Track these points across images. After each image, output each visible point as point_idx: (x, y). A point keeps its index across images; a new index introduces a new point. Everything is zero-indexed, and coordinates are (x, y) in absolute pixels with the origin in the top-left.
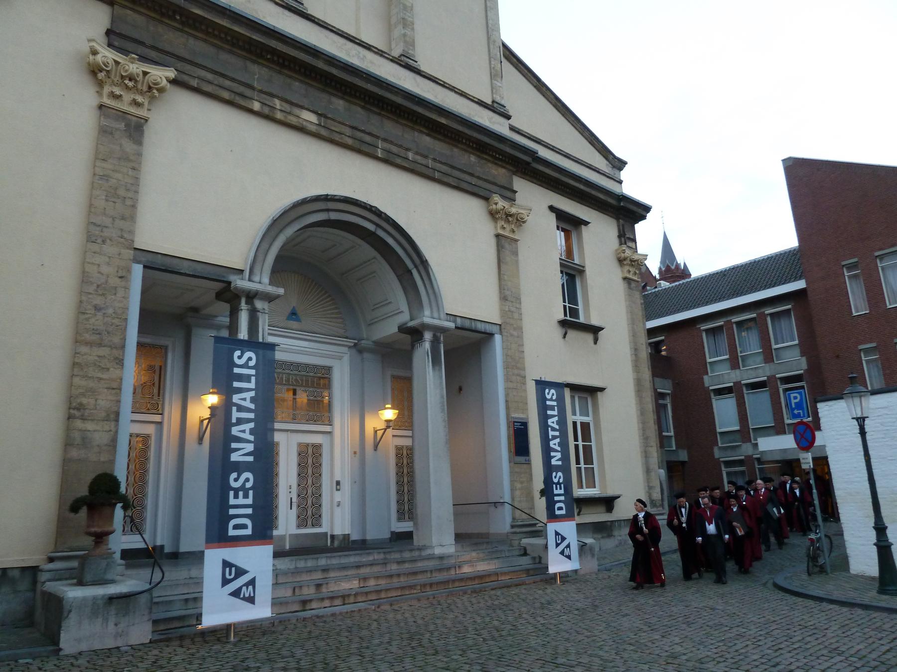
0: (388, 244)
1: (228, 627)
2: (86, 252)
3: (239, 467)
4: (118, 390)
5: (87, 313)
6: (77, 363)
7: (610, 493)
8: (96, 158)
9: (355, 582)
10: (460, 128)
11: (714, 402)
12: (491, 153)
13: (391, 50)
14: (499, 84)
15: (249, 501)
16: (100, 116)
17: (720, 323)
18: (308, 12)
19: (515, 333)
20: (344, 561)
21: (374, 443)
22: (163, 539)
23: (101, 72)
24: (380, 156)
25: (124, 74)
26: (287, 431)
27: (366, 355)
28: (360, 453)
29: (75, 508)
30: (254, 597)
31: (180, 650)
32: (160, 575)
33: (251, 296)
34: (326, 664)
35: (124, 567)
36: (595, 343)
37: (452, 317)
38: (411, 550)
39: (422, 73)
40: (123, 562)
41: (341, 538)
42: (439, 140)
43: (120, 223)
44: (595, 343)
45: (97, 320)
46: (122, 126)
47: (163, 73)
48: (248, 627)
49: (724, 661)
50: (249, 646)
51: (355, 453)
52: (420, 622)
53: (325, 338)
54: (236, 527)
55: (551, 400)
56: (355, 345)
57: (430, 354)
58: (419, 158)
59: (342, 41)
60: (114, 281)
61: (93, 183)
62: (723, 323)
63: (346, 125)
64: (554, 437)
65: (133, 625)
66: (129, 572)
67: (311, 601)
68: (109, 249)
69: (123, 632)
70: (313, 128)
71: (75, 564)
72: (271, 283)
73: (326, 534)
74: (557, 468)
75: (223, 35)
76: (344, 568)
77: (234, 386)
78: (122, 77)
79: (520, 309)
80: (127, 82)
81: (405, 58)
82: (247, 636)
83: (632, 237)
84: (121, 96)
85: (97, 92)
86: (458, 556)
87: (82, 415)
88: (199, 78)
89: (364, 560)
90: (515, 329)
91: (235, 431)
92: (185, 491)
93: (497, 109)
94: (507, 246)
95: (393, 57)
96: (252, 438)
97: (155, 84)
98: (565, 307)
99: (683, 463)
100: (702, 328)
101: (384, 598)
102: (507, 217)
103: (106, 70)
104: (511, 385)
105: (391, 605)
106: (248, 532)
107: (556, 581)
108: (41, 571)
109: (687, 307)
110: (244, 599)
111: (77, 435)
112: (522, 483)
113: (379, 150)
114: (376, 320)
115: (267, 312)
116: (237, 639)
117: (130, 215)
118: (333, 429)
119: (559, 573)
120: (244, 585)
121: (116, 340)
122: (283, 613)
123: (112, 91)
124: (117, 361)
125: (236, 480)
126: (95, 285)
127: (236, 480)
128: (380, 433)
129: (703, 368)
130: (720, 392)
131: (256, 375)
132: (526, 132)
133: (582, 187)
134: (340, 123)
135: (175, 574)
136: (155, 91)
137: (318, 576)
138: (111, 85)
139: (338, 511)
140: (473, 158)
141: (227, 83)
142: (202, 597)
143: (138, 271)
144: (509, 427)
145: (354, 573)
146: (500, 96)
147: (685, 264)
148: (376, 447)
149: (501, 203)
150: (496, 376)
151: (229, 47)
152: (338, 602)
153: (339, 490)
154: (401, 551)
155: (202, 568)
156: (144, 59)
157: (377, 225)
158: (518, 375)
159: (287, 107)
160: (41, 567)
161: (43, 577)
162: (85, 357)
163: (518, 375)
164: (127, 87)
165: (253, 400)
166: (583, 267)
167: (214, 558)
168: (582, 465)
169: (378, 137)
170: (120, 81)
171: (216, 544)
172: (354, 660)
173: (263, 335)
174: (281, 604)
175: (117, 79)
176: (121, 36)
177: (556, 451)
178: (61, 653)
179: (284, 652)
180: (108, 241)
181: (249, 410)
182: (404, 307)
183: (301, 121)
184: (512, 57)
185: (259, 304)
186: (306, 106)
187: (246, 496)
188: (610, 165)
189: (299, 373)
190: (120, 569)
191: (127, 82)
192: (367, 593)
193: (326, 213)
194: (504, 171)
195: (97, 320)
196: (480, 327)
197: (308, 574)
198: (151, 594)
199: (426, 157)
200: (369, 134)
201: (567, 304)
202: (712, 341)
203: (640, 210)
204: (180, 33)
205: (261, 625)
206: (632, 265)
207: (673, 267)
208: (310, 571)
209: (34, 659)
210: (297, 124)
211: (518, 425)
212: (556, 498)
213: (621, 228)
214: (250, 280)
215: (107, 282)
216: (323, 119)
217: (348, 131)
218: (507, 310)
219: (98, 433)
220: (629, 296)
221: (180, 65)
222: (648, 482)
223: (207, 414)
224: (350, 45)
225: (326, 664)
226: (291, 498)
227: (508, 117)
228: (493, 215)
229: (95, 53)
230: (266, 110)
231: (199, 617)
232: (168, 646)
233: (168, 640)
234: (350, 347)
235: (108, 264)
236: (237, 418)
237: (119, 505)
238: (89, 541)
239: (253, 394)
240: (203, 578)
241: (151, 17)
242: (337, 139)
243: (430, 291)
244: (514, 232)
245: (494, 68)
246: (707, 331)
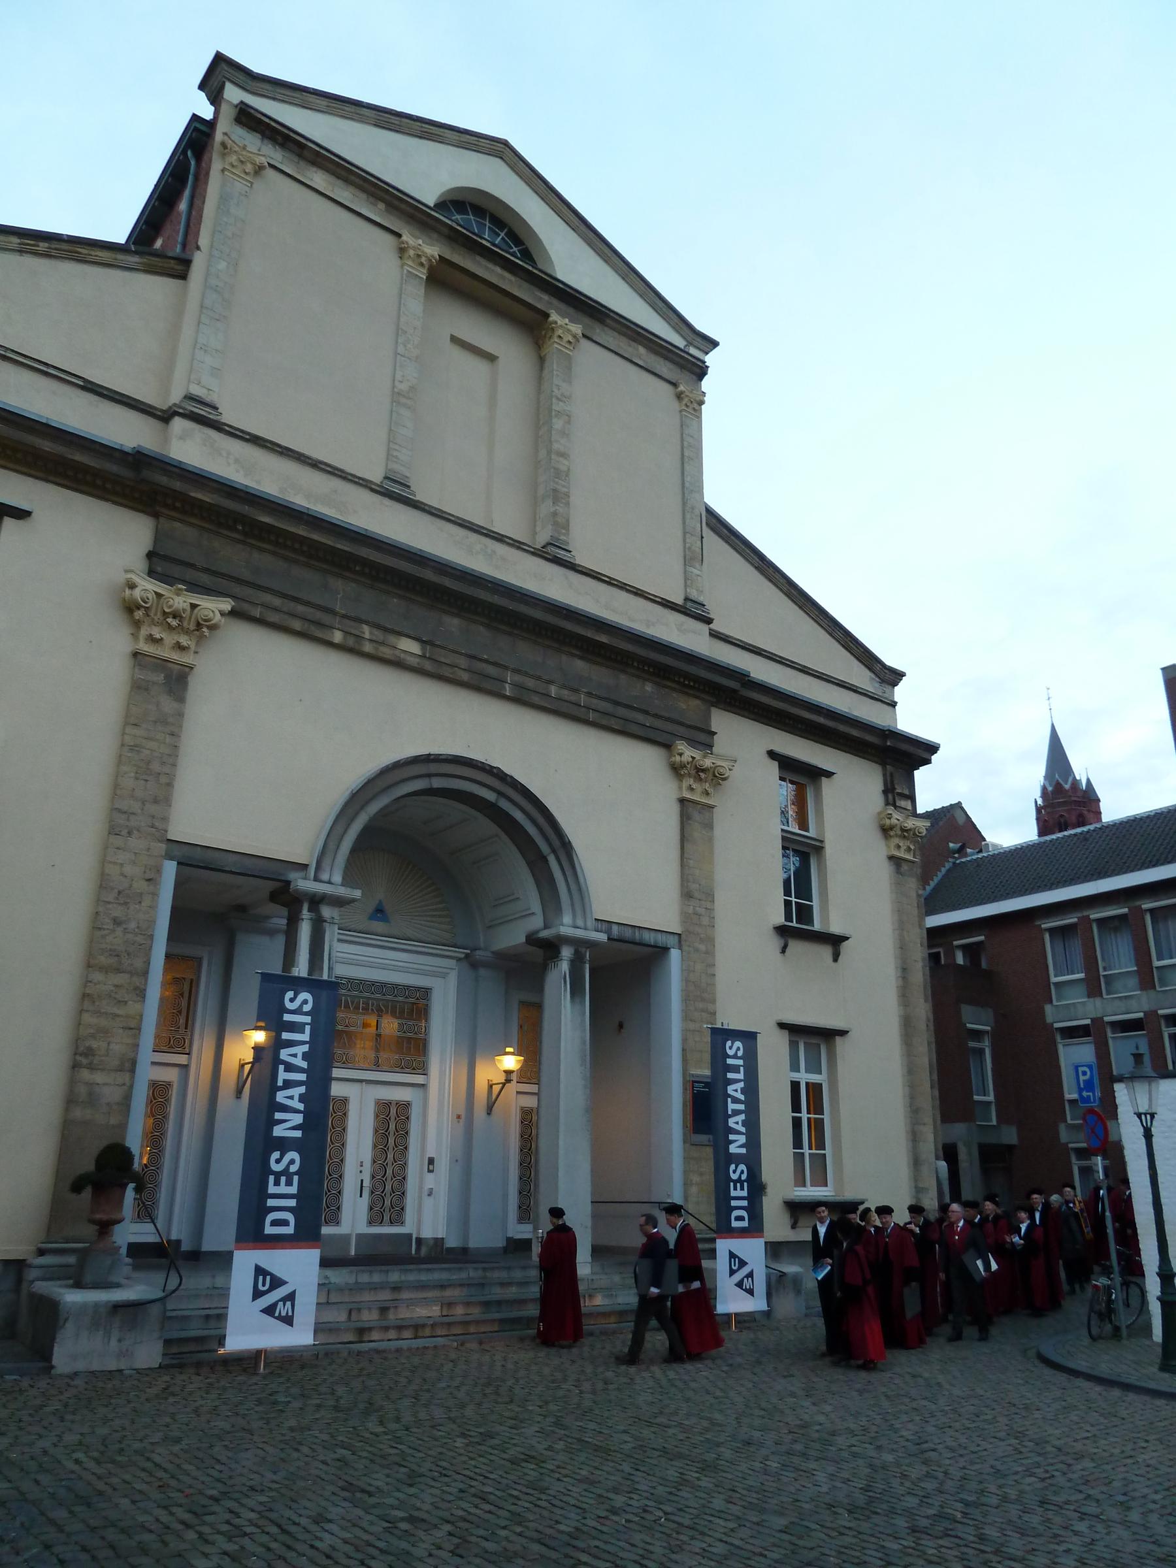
1: (259, 1353)
3: (283, 1145)
5: (104, 929)
6: (88, 995)
8: (126, 724)
9: (434, 1308)
11: (1061, 1048)
14: (696, 571)
15: (293, 1190)
16: (134, 666)
17: (1071, 920)
18: (417, 498)
19: (702, 947)
20: (424, 1277)
22: (179, 1231)
23: (139, 609)
25: (167, 610)
26: (361, 1081)
27: (482, 972)
28: (466, 1118)
29: (77, 1187)
33: (316, 901)
34: (370, 1404)
35: (131, 1267)
36: (835, 959)
37: (605, 925)
38: (524, 1268)
39: (577, 568)
41: (432, 1242)
43: (153, 809)
44: (835, 959)
46: (160, 678)
48: (283, 1357)
50: (281, 1380)
51: (459, 1117)
52: (510, 1366)
53: (424, 947)
54: (275, 1223)
55: (735, 1057)
56: (467, 956)
58: (565, 693)
59: (462, 532)
60: (140, 886)
61: (120, 756)
62: (1076, 920)
63: (461, 654)
64: (736, 1113)
66: (136, 1275)
67: (370, 1329)
68: (135, 843)
70: (413, 661)
71: (72, 1260)
72: (344, 884)
74: (738, 1159)
75: (297, 546)
76: (423, 1287)
77: (284, 1019)
78: (164, 613)
79: (710, 910)
80: (169, 620)
82: (281, 1368)
83: (906, 792)
85: (132, 634)
86: (593, 1280)
87: (91, 1063)
89: (454, 1277)
90: (702, 941)
91: (280, 1097)
94: (696, 816)
96: (301, 1107)
97: (206, 621)
98: (788, 904)
99: (1010, 1148)
100: (1043, 926)
101: (473, 1334)
102: (697, 772)
104: (692, 1026)
105: (481, 1343)
106: (289, 1230)
107: (730, 1327)
108: (30, 1266)
109: (1020, 891)
110: (280, 1318)
111: (82, 1090)
112: (701, 1174)
113: (507, 686)
116: (267, 1371)
117: (163, 798)
119: (735, 1314)
121: (138, 964)
123: (151, 635)
124: (138, 992)
125: (278, 1161)
126: (116, 891)
127: (278, 1161)
128: (496, 1089)
129: (1044, 991)
130: (1072, 1033)
131: (312, 1024)
132: (738, 640)
135: (197, 1281)
136: (205, 630)
137: (385, 1295)
138: (149, 626)
139: (428, 1202)
140: (649, 687)
141: (301, 609)
142: (227, 1314)
143: (170, 869)
144: (685, 1089)
147: (1088, 781)
149: (687, 752)
152: (407, 1334)
154: (509, 1268)
155: (229, 1276)
156: (195, 587)
159: (379, 635)
161: (32, 1274)
162: (97, 986)
166: (822, 842)
167: (245, 1261)
169: (506, 668)
170: (162, 618)
171: (251, 1244)
173: (330, 955)
174: (330, 1330)
175: (158, 617)
177: (738, 1133)
178: (53, 1372)
179: (323, 1389)
181: (299, 1070)
182: (536, 906)
183: (397, 652)
184: (722, 528)
185: (326, 912)
190: (126, 1270)
192: (449, 1324)
194: (697, 702)
196: (649, 938)
197: (372, 1292)
198: (165, 1305)
201: (793, 899)
203: (919, 751)
206: (905, 837)
207: (1067, 787)
210: (392, 658)
211: (699, 1087)
213: (889, 779)
214: (316, 879)
216: (428, 647)
217: (463, 662)
219: (107, 1085)
220: (898, 885)
221: (238, 590)
222: (916, 1180)
223: (249, 1056)
225: (370, 1404)
226: (362, 1181)
227: (709, 621)
228: (677, 770)
229: (132, 586)
230: (351, 642)
231: (221, 1340)
232: (181, 1373)
233: (181, 1366)
234: (459, 960)
236: (284, 1080)
237: (131, 1186)
238: (90, 1231)
239: (306, 1048)
240: (230, 1288)
241: (204, 528)
243: (573, 887)
244: (707, 794)
245: (689, 548)
246: (1052, 931)
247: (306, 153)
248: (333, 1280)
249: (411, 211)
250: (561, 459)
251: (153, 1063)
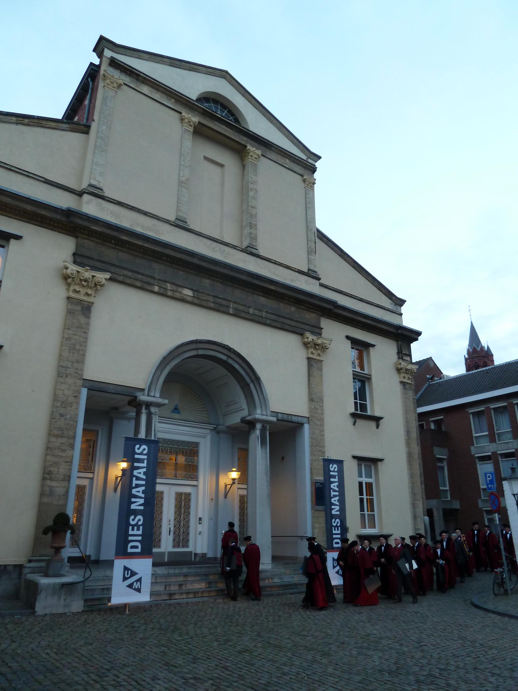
0: (235, 367)
1: (125, 605)
2: (57, 383)
3: (135, 513)
4: (70, 463)
6: (49, 447)
7: (385, 532)
8: (64, 328)
10: (284, 291)
11: (478, 465)
12: (305, 305)
13: (242, 247)
15: (140, 532)
16: (68, 303)
17: (482, 408)
19: (318, 423)
21: (225, 493)
22: (90, 551)
24: (231, 313)
25: (82, 278)
27: (221, 435)
28: (215, 500)
29: (45, 532)
30: (140, 588)
31: (98, 616)
32: (90, 573)
33: (148, 405)
34: (175, 627)
35: (69, 567)
36: (377, 427)
40: (68, 564)
42: (271, 299)
44: (377, 427)
45: (61, 422)
46: (79, 308)
47: (103, 276)
48: (137, 607)
49: (447, 651)
51: (212, 499)
54: (132, 547)
55: (334, 471)
56: (215, 428)
60: (71, 399)
62: (484, 408)
64: (335, 496)
65: (74, 601)
66: (71, 571)
67: (174, 594)
68: (70, 380)
69: (68, 604)
70: (189, 299)
71: (43, 564)
72: (161, 397)
73: (192, 552)
78: (81, 280)
79: (322, 406)
80: (83, 283)
81: (250, 249)
83: (407, 353)
84: (80, 291)
88: (123, 275)
91: (134, 491)
92: (105, 522)
93: (312, 274)
94: (315, 365)
95: (242, 249)
96: (143, 496)
98: (356, 403)
99: (457, 510)
100: (469, 411)
102: (315, 346)
103: (72, 277)
106: (139, 550)
108: (25, 567)
110: (135, 589)
111: (47, 489)
112: (320, 523)
114: (229, 413)
115: (157, 414)
117: (81, 360)
118: (198, 483)
120: (135, 581)
121: (71, 433)
122: (158, 600)
125: (133, 520)
127: (133, 520)
128: (229, 487)
130: (483, 459)
133: (369, 322)
134: (206, 294)
135: (98, 573)
136: (98, 286)
137: (181, 579)
139: (199, 537)
140: (293, 309)
141: (140, 277)
142: (112, 588)
143: (84, 392)
145: (194, 579)
146: (313, 266)
147: (488, 347)
148: (226, 496)
149: (310, 337)
150: (304, 452)
151: (142, 255)
152: (191, 596)
155: (112, 571)
158: (320, 451)
159: (174, 288)
160: (25, 565)
161: (26, 571)
163: (320, 451)
164: (83, 286)
165: (145, 473)
166: (370, 376)
167: (119, 564)
168: (366, 512)
169: (230, 301)
172: (191, 626)
173: (155, 427)
175: (78, 281)
176: (81, 256)
177: (336, 505)
178: (36, 614)
180: (69, 376)
181: (142, 479)
182: (245, 406)
183: (182, 295)
186: (186, 286)
187: (138, 529)
188: (393, 303)
189: (178, 447)
190: (67, 568)
191: (83, 283)
193: (196, 350)
194: (314, 315)
195: (61, 422)
196: (295, 419)
198: (84, 584)
199: (261, 311)
200: (224, 299)
201: (358, 401)
202: (477, 420)
203: (413, 334)
204: (114, 250)
205: (144, 606)
207: (479, 349)
208: (176, 576)
209: (22, 616)
210: (180, 298)
211: (318, 485)
212: (334, 536)
213: (399, 348)
214: (148, 395)
215: (67, 399)
217: (211, 299)
218: (313, 407)
219: (58, 488)
221: (112, 269)
223: (120, 474)
224: (215, 244)
225: (175, 627)
226: (170, 528)
227: (319, 279)
228: (306, 345)
229: (66, 268)
230: (162, 291)
231: (109, 600)
232: (92, 614)
234: (211, 430)
235: (69, 389)
237: (69, 531)
238: (52, 551)
239: (145, 470)
242: (205, 305)
243: (261, 397)
244: (319, 355)
246: (473, 414)
247: (140, 78)
248: (158, 572)
249: (186, 102)
251: (78, 477)
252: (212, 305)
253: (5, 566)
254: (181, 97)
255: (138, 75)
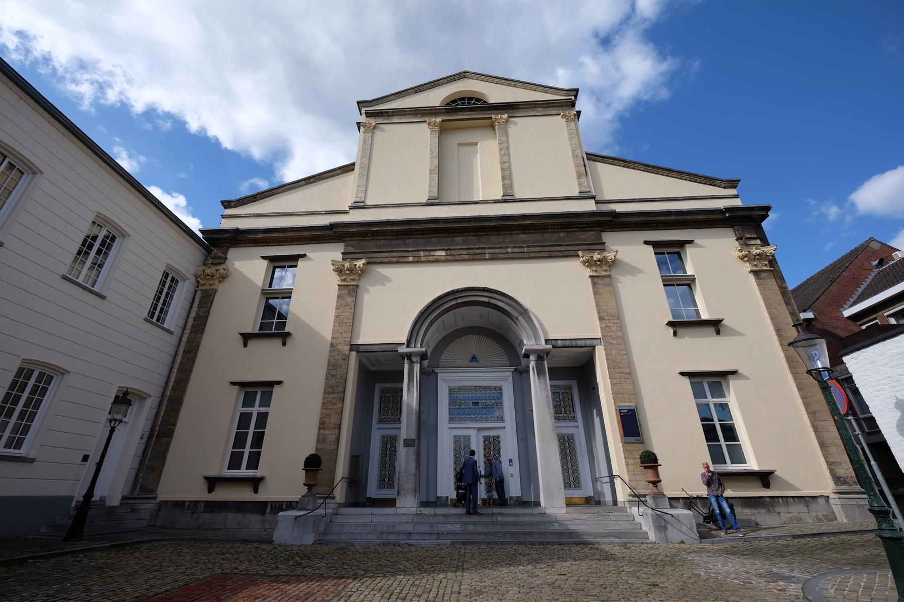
24: (487, 257)
56: (516, 370)
57: (535, 369)
70: (443, 258)
87: (324, 427)
88: (381, 257)
112: (635, 459)
113: (487, 255)
141: (395, 254)
153: (512, 465)
157: (490, 297)
159: (427, 253)
183: (436, 257)
230: (416, 259)
247: (390, 114)
248: (423, 512)
249: (429, 111)
250: (505, 164)
251: (378, 428)
252: (466, 257)
253: (291, 502)
254: (424, 110)
255: (387, 112)
